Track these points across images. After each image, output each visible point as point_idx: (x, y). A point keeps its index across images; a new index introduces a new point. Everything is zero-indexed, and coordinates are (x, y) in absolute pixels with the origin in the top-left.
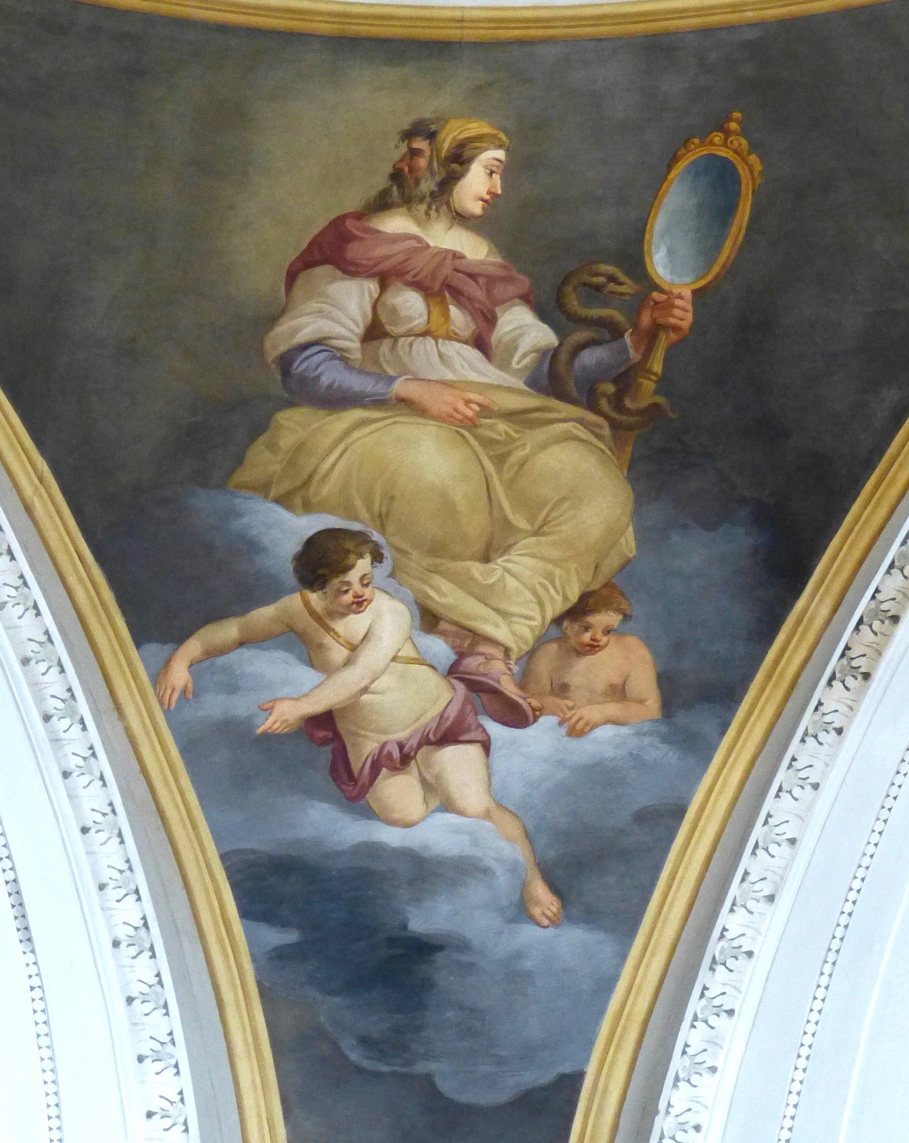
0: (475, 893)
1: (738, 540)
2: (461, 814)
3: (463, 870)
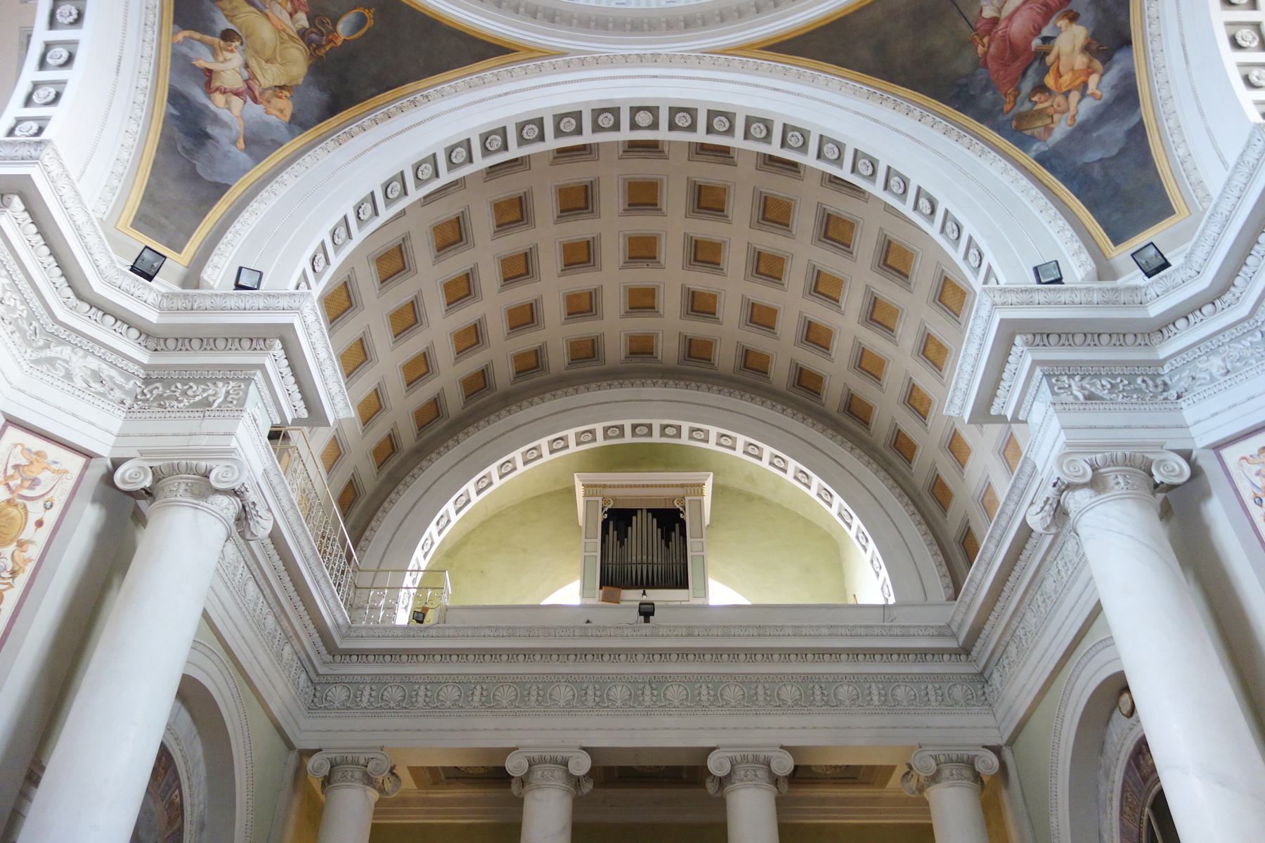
0: (226, 132)
1: (325, 97)
2: (232, 114)
3: (225, 125)
